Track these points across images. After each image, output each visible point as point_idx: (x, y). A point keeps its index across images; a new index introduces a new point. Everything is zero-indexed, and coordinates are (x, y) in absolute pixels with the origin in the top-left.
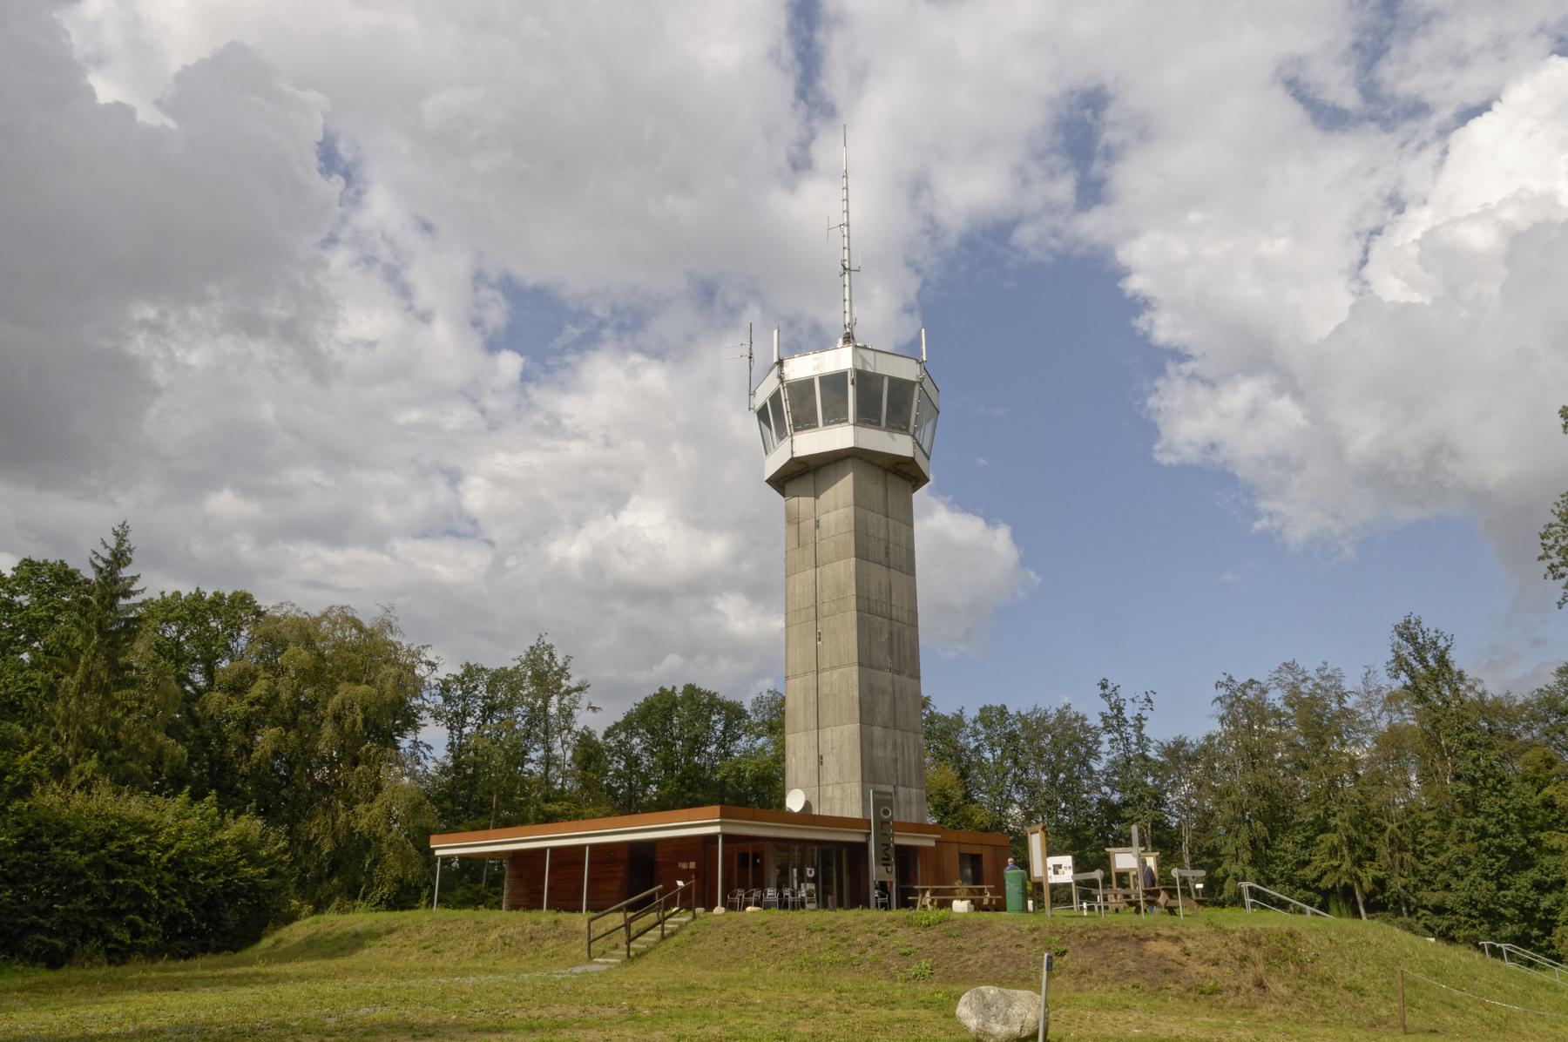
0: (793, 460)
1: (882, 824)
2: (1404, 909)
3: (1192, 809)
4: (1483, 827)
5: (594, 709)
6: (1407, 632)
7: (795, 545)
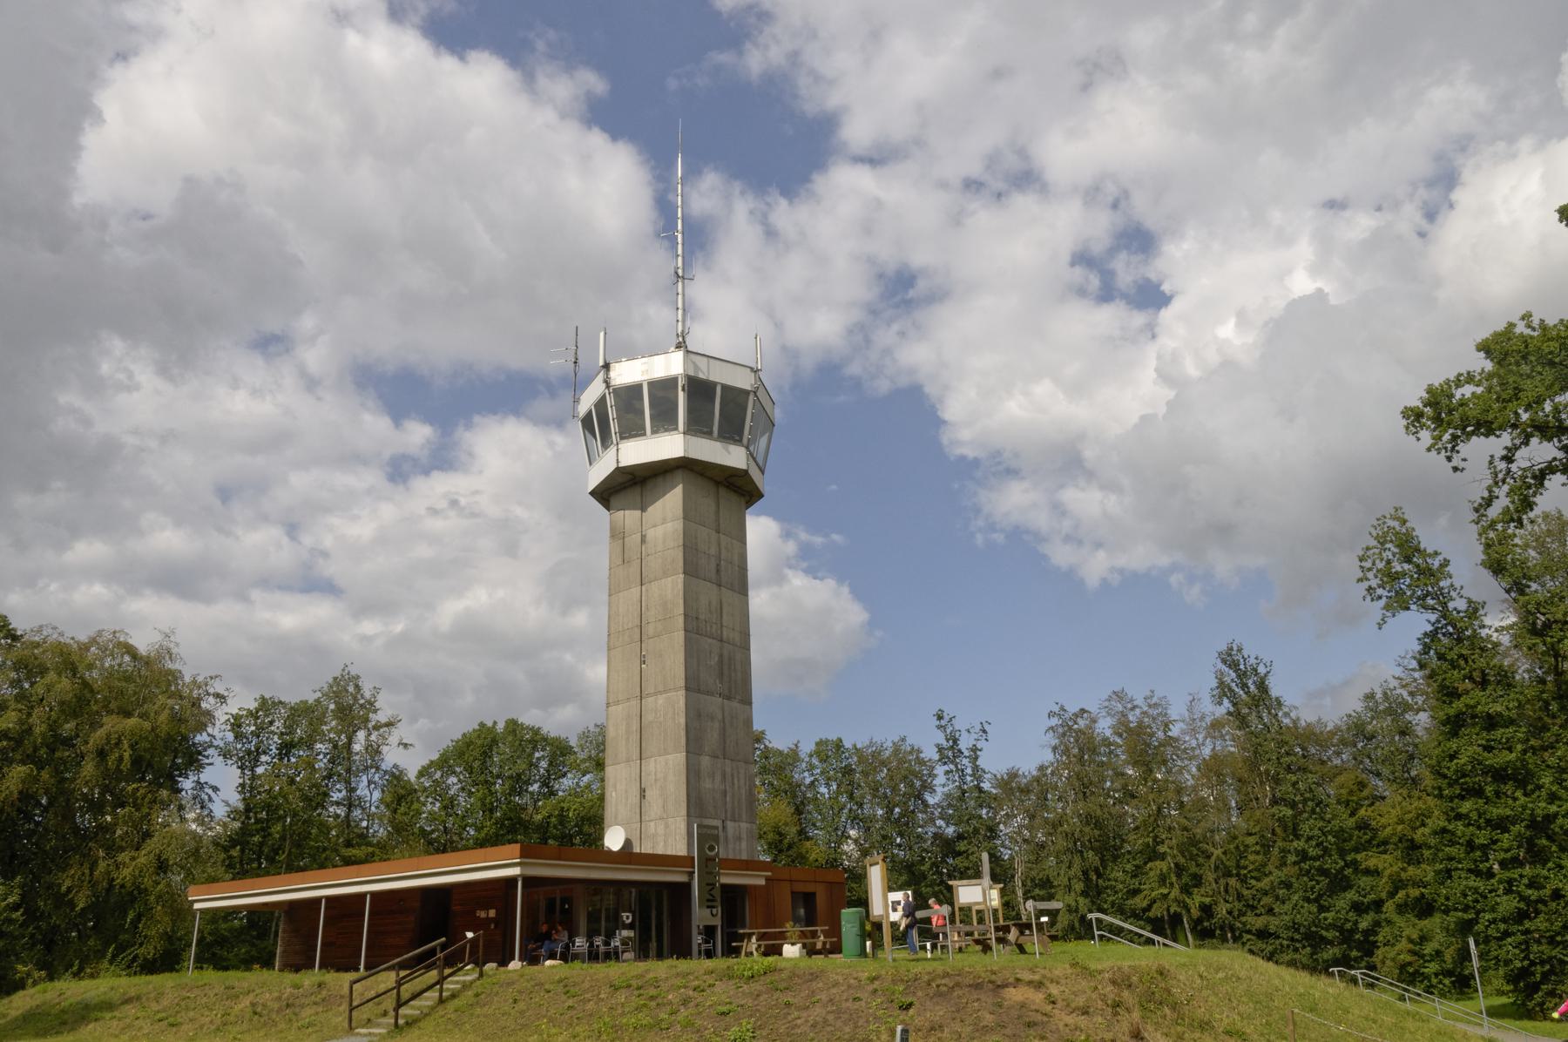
0: (618, 469)
1: (707, 861)
2: (1229, 935)
3: (1025, 841)
4: (1303, 850)
5: (406, 745)
6: (1230, 658)
7: (620, 561)
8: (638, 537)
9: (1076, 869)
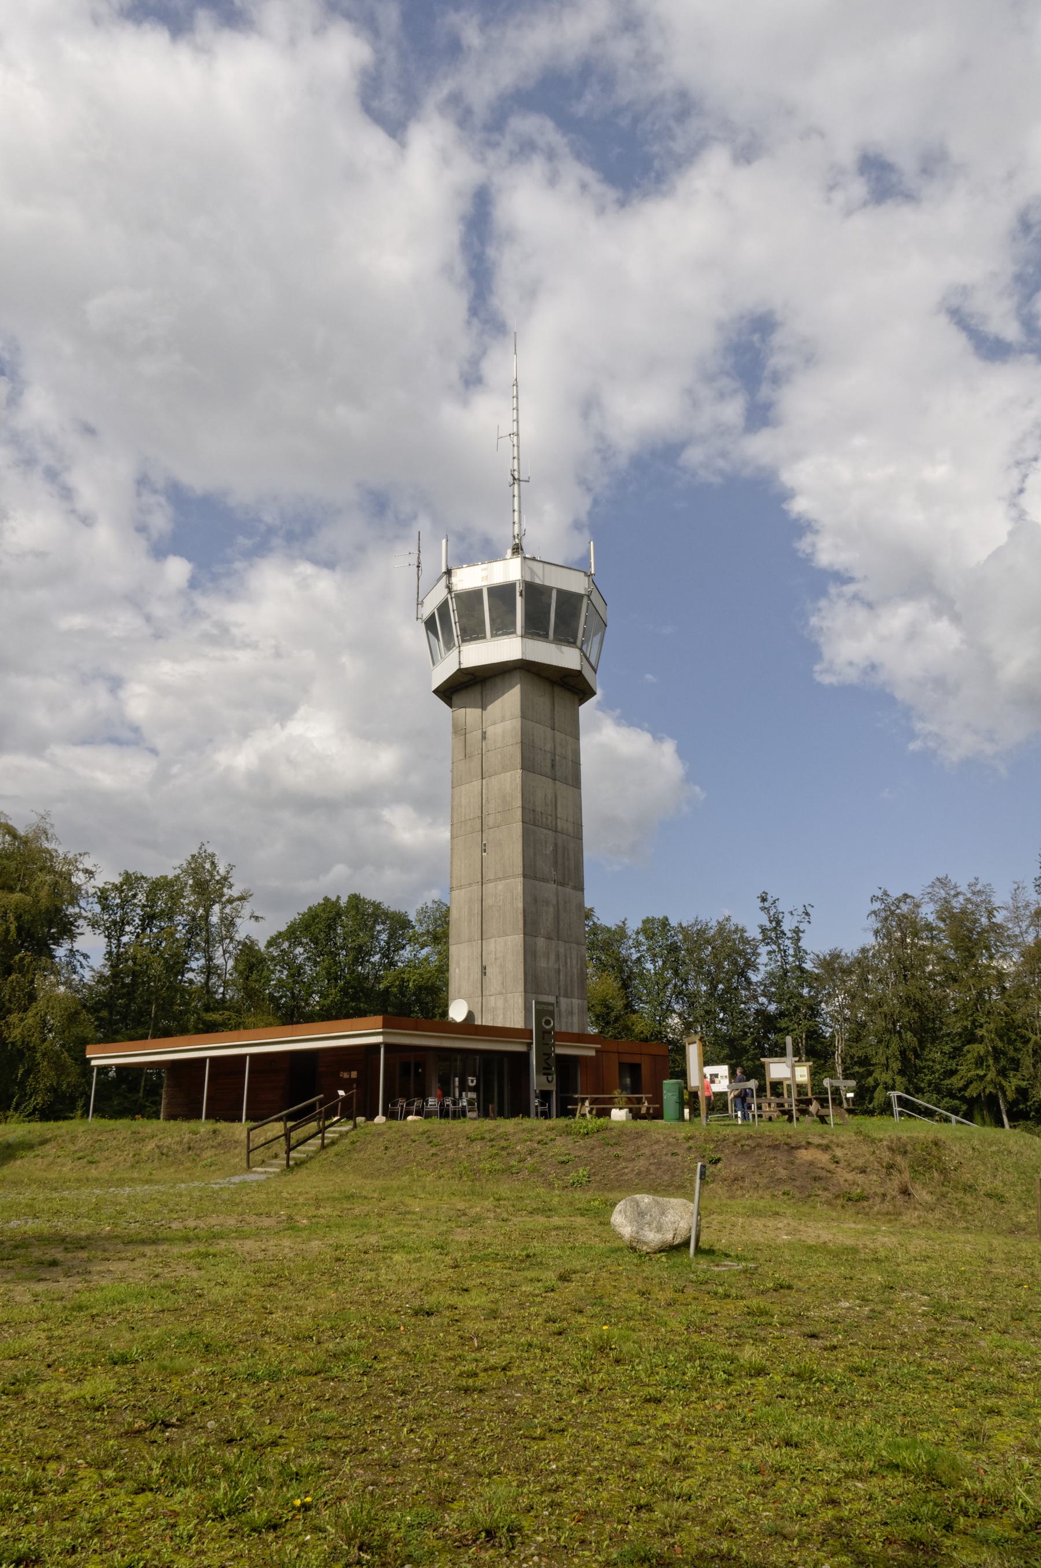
0: (460, 670)
1: (544, 1035)
3: (846, 1020)
5: (257, 918)
7: (462, 756)
8: (479, 733)
9: (895, 1046)
